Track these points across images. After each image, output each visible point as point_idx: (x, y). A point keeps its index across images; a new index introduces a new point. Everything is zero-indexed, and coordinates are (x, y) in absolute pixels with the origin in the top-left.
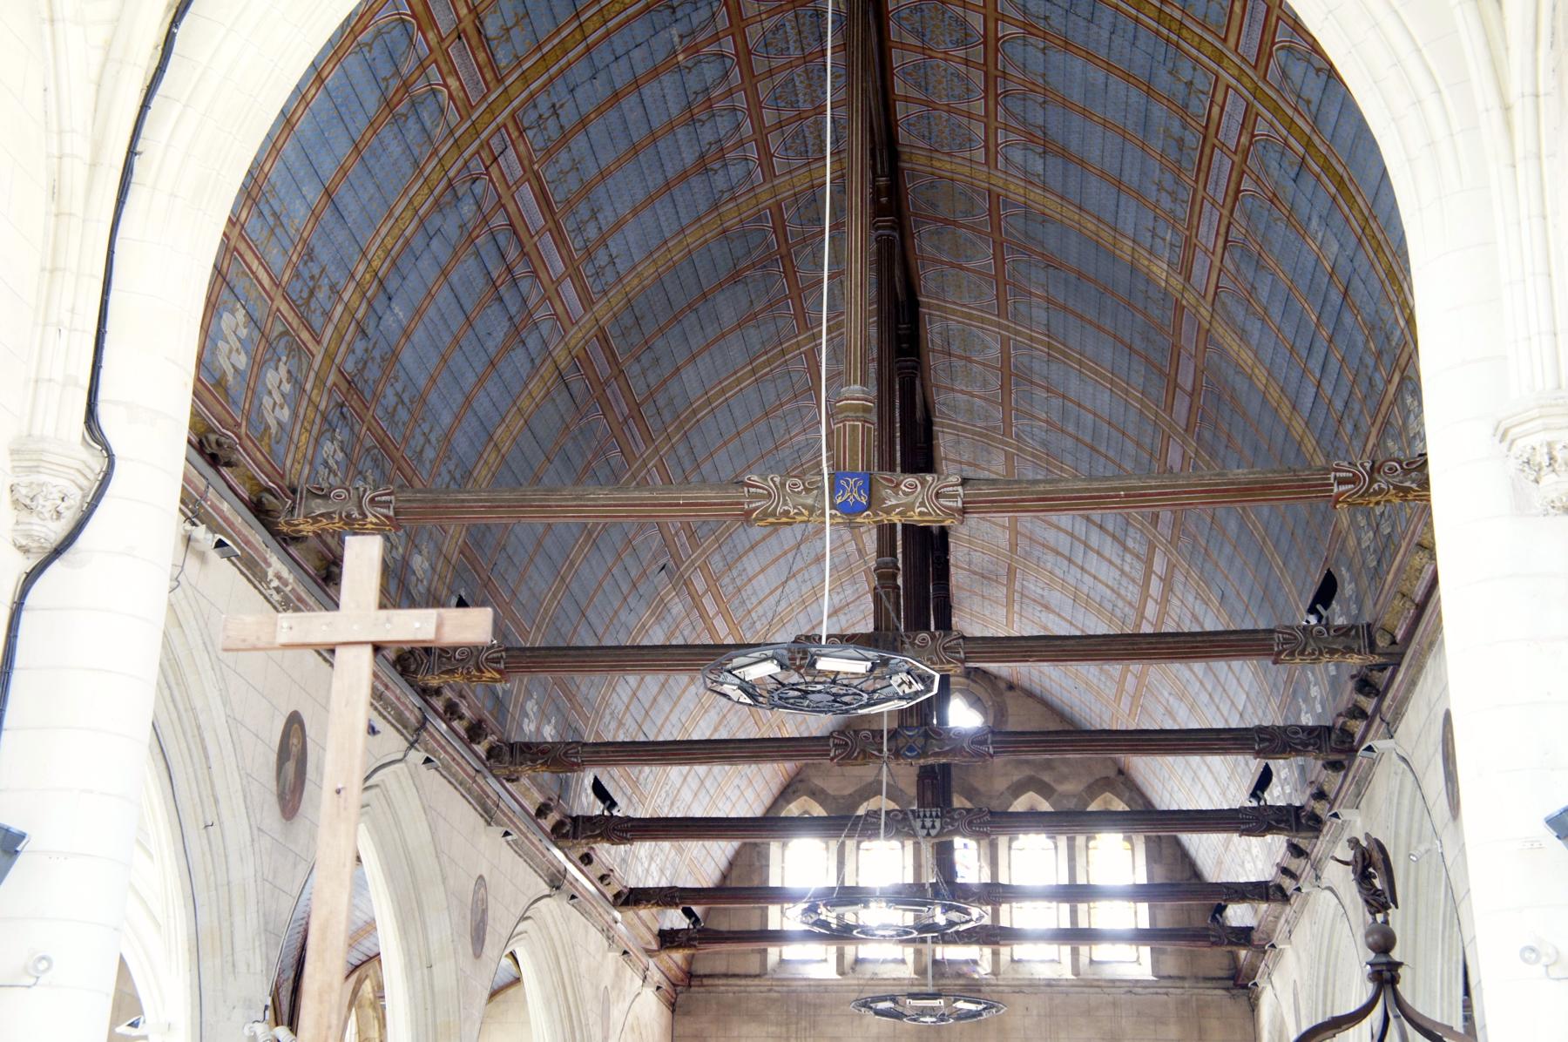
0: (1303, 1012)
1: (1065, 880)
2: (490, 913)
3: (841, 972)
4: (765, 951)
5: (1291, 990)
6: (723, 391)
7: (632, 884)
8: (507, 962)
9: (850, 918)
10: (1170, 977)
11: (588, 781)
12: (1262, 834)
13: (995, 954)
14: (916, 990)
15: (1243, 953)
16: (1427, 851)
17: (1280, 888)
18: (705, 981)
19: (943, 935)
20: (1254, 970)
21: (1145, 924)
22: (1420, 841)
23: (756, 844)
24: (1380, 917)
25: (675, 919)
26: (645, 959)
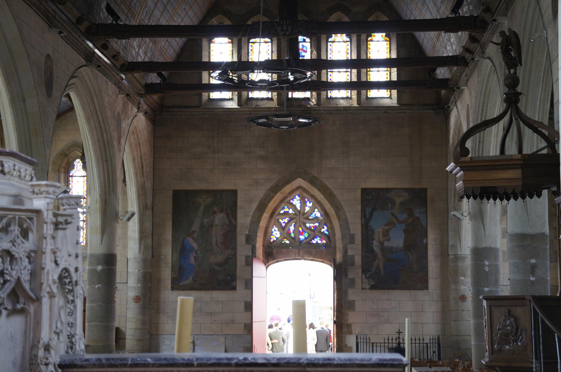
0: (471, 119)
1: (354, 57)
3: (239, 104)
4: (201, 94)
5: (466, 109)
6: (366, 343)
7: (130, 59)
8: (64, 99)
9: (244, 77)
10: (406, 105)
11: (103, 5)
13: (319, 95)
14: (278, 113)
15: (443, 92)
16: (539, 37)
19: (293, 85)
20: (448, 100)
21: (394, 78)
22: (536, 32)
24: (512, 71)
25: (153, 78)
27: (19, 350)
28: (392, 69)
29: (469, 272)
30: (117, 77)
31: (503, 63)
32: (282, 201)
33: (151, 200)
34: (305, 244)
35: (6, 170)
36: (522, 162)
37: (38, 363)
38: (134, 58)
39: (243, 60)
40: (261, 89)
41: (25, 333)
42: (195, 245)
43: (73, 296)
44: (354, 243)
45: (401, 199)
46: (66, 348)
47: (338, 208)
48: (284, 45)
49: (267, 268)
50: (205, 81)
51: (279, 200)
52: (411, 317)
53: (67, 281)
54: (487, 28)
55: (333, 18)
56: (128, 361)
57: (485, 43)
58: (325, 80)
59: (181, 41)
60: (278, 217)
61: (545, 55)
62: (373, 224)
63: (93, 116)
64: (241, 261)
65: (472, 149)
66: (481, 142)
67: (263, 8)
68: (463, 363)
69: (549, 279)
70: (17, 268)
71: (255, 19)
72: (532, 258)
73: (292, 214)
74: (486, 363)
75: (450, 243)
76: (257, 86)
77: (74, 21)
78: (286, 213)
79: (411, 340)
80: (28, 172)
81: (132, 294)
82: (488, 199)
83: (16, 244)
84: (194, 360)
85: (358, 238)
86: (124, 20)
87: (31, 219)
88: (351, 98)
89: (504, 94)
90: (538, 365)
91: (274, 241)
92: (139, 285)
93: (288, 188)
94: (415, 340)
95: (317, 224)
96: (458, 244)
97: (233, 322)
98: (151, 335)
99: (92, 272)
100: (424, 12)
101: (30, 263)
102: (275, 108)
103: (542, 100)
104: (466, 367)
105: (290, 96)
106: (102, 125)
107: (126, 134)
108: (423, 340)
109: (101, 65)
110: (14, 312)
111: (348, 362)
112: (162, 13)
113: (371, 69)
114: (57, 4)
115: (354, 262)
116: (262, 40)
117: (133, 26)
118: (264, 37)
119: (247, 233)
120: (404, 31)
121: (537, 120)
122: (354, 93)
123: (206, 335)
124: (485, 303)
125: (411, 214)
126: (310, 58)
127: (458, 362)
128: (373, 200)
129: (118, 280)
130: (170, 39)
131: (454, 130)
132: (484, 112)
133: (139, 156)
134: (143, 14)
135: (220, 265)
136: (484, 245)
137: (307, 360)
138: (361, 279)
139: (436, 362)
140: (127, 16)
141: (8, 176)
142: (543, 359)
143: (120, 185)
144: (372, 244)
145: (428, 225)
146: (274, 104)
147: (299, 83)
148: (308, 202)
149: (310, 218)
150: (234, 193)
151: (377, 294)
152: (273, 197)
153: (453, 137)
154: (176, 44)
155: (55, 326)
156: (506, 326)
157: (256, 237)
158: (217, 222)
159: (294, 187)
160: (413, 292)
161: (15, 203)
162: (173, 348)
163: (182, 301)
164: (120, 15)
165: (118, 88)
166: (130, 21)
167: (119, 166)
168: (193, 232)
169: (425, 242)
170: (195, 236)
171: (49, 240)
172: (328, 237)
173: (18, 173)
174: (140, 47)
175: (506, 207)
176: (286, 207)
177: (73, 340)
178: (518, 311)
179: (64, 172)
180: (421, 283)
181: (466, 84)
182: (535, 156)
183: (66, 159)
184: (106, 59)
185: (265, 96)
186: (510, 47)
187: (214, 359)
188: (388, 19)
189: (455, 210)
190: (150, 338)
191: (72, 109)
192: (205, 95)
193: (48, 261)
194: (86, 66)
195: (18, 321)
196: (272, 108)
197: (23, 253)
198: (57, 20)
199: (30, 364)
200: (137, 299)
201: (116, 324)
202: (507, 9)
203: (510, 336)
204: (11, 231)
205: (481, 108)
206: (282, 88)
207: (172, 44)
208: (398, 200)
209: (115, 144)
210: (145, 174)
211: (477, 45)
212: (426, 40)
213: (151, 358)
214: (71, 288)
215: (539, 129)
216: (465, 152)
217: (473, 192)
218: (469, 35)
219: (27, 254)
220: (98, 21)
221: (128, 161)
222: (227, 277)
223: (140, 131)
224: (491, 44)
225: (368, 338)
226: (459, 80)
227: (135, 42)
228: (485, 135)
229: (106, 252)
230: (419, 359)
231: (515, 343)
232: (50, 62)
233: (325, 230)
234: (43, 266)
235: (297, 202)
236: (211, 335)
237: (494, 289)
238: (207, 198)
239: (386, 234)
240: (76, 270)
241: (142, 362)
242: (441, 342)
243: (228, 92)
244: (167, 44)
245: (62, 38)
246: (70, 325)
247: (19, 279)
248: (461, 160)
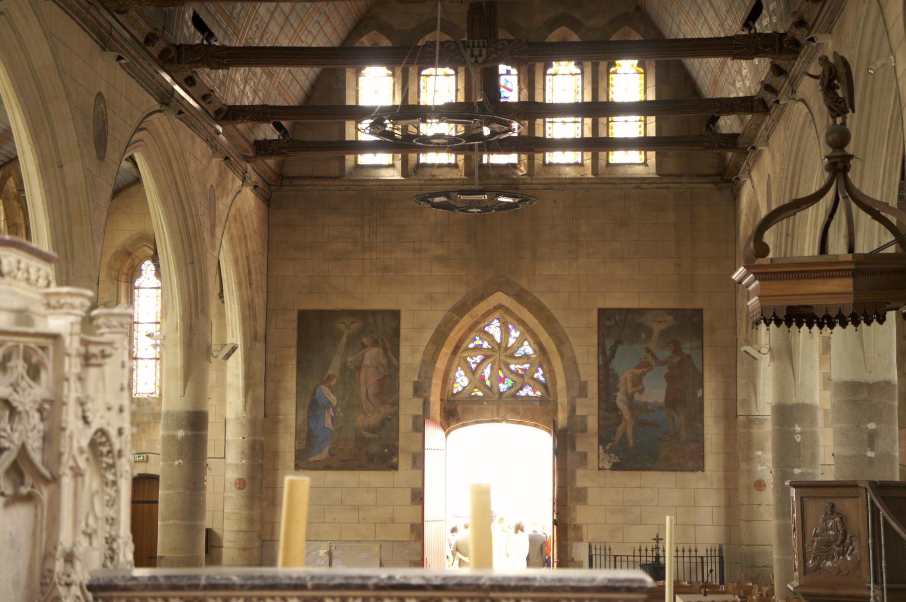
0: (773, 199)
1: (588, 98)
2: (110, 123)
3: (404, 173)
4: (344, 157)
7: (230, 102)
8: (126, 165)
9: (412, 130)
10: (670, 175)
11: (188, 15)
12: (751, 57)
13: (531, 159)
14: (466, 187)
15: (730, 154)
16: (883, 66)
17: (763, 102)
18: (294, 182)
20: (738, 168)
21: (652, 132)
22: (878, 58)
23: (334, 70)
24: (839, 120)
25: (267, 132)
26: (243, 164)
27: (23, 561)
28: (648, 118)
29: (769, 444)
30: (209, 129)
31: (826, 109)
32: (471, 329)
33: (264, 325)
34: (507, 397)
35: (5, 269)
36: (854, 267)
37: (55, 584)
38: (236, 99)
39: (410, 103)
40: (438, 148)
41: (34, 533)
42: (333, 398)
43: (115, 474)
44: (586, 396)
45: (662, 327)
46: (103, 558)
47: (560, 341)
48: (476, 79)
49: (446, 435)
50: (350, 136)
51: (467, 327)
52: (677, 514)
53: (105, 449)
54: (799, 53)
55: (554, 37)
56: (200, 579)
57: (797, 76)
58: (542, 136)
59: (312, 72)
60: (465, 355)
61: (893, 96)
62: (616, 365)
63: (170, 192)
64: (405, 424)
65: (775, 246)
66: (790, 234)
67: (442, 20)
68: (760, 589)
69: (897, 454)
70: (20, 427)
71: (428, 38)
72: (870, 420)
73: (488, 349)
74: (795, 588)
75: (740, 397)
76: (431, 143)
77: (142, 41)
78: (479, 348)
79: (677, 551)
80: (42, 273)
81: (232, 475)
82: (799, 326)
83: (19, 389)
84: (308, 579)
85: (593, 388)
86: (221, 39)
87: (44, 348)
89: (826, 157)
90: (878, 592)
91: (458, 393)
92: (244, 461)
93: (481, 308)
94: (683, 551)
95: (527, 366)
96: (753, 397)
97: (392, 520)
98: (263, 541)
99: (169, 440)
100: (699, 27)
101: (42, 420)
102: (460, 179)
103: (888, 167)
104: (764, 595)
105: (485, 161)
106: (186, 206)
107: (224, 220)
108: (696, 551)
109: (184, 110)
110: (16, 499)
111: (558, 584)
112: (282, 28)
113: (615, 118)
114: (115, 13)
115: (586, 426)
116: (441, 71)
117: (235, 48)
118: (443, 66)
119: (416, 379)
120: (668, 57)
121: (878, 199)
122: (588, 155)
123: (349, 541)
124: (793, 492)
125: (677, 350)
126: (516, 100)
127: (751, 588)
128: (616, 327)
129: (210, 453)
130: (294, 70)
131: (747, 216)
132: (795, 187)
133: (244, 255)
134: (251, 29)
135: (372, 430)
136: (794, 400)
137: (491, 579)
138: (596, 454)
139: (715, 586)
140: (225, 32)
141: (7, 279)
142: (887, 582)
143: (214, 301)
144: (615, 397)
145: (705, 368)
146: (459, 174)
147: (499, 140)
148: (513, 331)
149: (516, 355)
150: (395, 315)
151: (622, 477)
152: (457, 322)
153: (746, 228)
154: (304, 77)
155: (83, 525)
156: (828, 530)
157: (430, 386)
158: (367, 361)
159: (491, 307)
160: (680, 475)
161: (19, 322)
162: (296, 560)
163: (292, 483)
165: (212, 147)
166: (230, 40)
167: (213, 270)
168: (330, 378)
169: (699, 395)
170: (333, 383)
171: (74, 384)
172: (545, 386)
173: (26, 275)
174: (246, 82)
175: (829, 338)
176: (478, 338)
177: (115, 546)
178: (847, 506)
179: (126, 282)
180: (690, 459)
182: (874, 256)
183: (129, 261)
184: (191, 101)
185: (445, 162)
186: (836, 82)
187: (341, 577)
188: (642, 38)
189: (748, 343)
190: (262, 543)
191: (138, 180)
192: (349, 159)
193: (71, 418)
194: (160, 111)
195: (22, 514)
196: (457, 179)
197: (31, 404)
198: (115, 39)
199: (42, 584)
200: (241, 484)
201: (207, 523)
202: (832, 22)
203: (834, 546)
204: (12, 368)
205: (789, 182)
206: (471, 148)
207: (298, 78)
208: (657, 328)
209: (207, 236)
210: (254, 286)
211: (783, 79)
212: (702, 72)
213: (238, 576)
214: (110, 461)
215: (883, 214)
216: (762, 250)
217: (774, 315)
218: (771, 63)
219: (37, 406)
220: (180, 41)
221: (227, 264)
222: (381, 448)
223: (246, 217)
224: (807, 77)
225: (607, 548)
227: (239, 74)
228: (797, 222)
229: (192, 409)
230: (690, 582)
231: (841, 557)
232: (102, 104)
233: (539, 375)
234: (63, 425)
235: (494, 329)
236: (358, 541)
237: (810, 471)
238: (352, 323)
239: (637, 382)
240: (120, 432)
241: (223, 582)
242: (724, 555)
243: (387, 155)
244: (290, 77)
245: (122, 67)
246: (110, 522)
247: (23, 447)
248: (756, 263)
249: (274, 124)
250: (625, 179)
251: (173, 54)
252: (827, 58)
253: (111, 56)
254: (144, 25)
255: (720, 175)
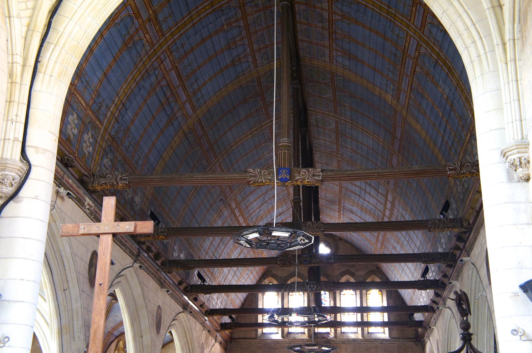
1: (359, 305)
3: (283, 336)
5: (436, 342)
7: (211, 307)
8: (168, 334)
9: (286, 319)
11: (196, 273)
12: (425, 289)
13: (336, 330)
14: (308, 343)
15: (420, 330)
18: (237, 340)
20: (423, 336)
21: (386, 320)
22: (479, 292)
24: (465, 318)
25: (226, 319)
48: (312, 297)
50: (260, 320)
77: (177, 284)
86: (208, 282)
88: (357, 333)
105: (316, 331)
122: (360, 329)
130: (237, 294)
132: (449, 345)
146: (306, 337)
164: (206, 278)
165: (203, 326)
174: (218, 299)
181: (435, 325)
192: (260, 331)
194: (183, 312)
202: (458, 276)
220: (192, 283)
226: (430, 322)
227: (215, 296)
249: (229, 316)
250: (376, 339)
251: (189, 289)
252: (457, 292)
253: (165, 290)
254: (178, 278)
255: (417, 338)
